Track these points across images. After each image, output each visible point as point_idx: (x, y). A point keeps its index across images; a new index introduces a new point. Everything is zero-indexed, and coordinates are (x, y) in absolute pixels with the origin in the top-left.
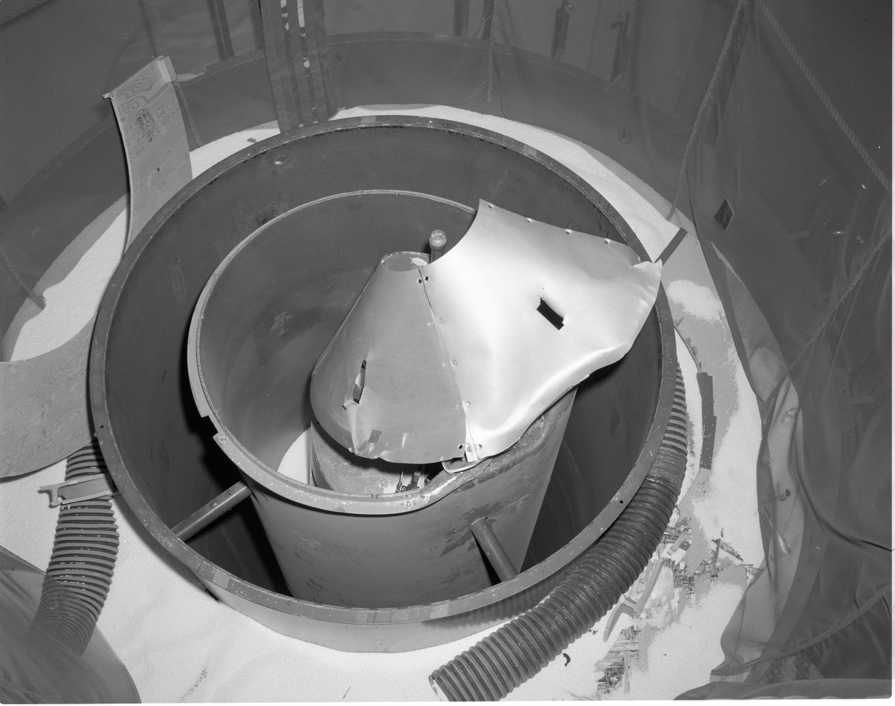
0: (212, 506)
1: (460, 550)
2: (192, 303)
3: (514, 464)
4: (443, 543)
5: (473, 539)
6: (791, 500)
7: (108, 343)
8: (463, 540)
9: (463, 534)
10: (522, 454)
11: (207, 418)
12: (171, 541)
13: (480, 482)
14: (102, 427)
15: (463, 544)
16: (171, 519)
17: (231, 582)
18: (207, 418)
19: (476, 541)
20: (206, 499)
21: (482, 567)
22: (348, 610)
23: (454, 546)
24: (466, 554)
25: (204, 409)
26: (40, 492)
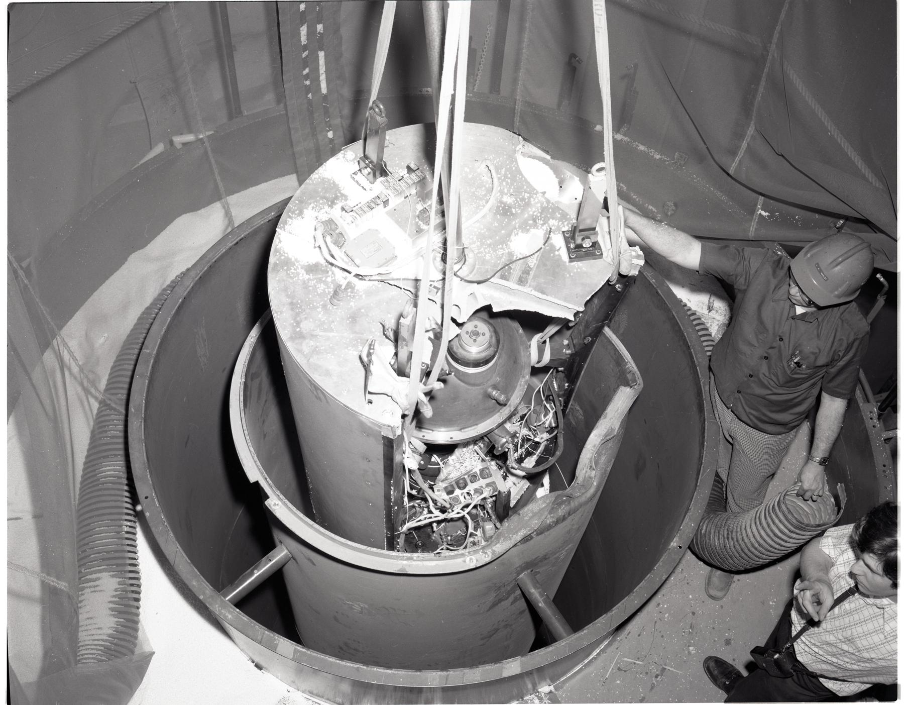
0: (252, 574)
1: (506, 604)
2: (233, 354)
3: (569, 514)
4: (491, 597)
5: (518, 592)
6: (494, 548)
7: (145, 411)
8: (512, 591)
9: (509, 588)
10: (577, 503)
11: (257, 483)
12: (229, 612)
13: (538, 534)
14: (146, 498)
15: (507, 598)
16: (221, 585)
17: (296, 651)
18: (257, 484)
19: (523, 593)
20: (253, 563)
21: (527, 616)
22: (418, 673)
23: (500, 601)
24: (514, 607)
25: (253, 472)
26: (637, 478)
